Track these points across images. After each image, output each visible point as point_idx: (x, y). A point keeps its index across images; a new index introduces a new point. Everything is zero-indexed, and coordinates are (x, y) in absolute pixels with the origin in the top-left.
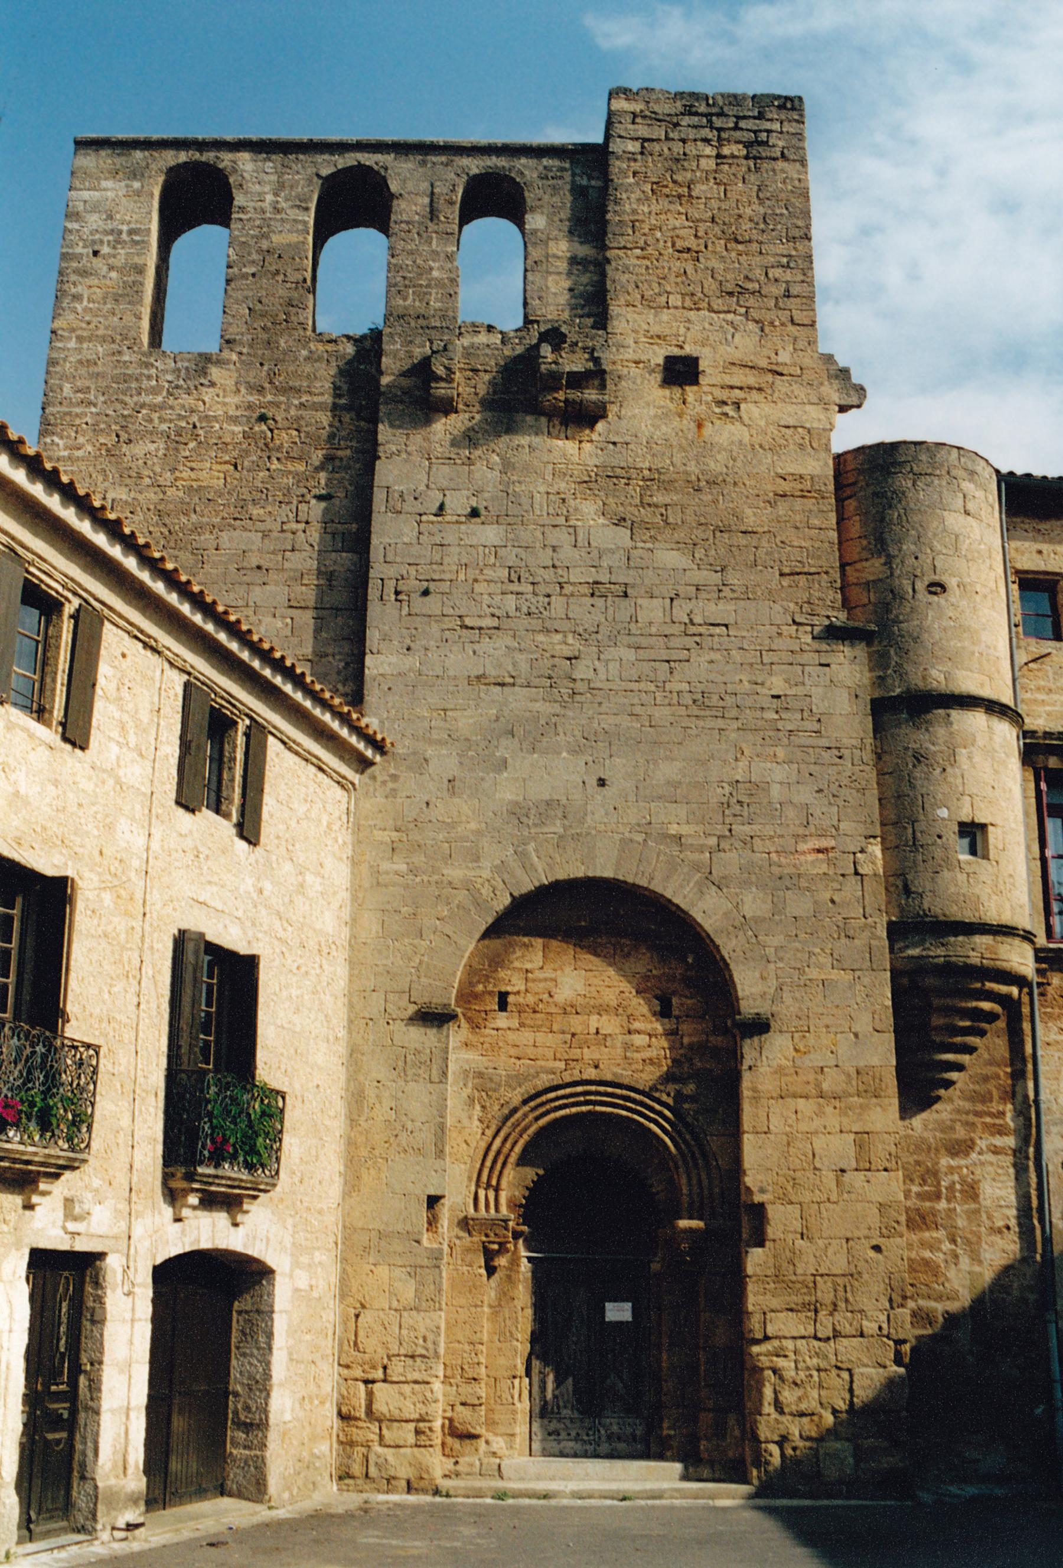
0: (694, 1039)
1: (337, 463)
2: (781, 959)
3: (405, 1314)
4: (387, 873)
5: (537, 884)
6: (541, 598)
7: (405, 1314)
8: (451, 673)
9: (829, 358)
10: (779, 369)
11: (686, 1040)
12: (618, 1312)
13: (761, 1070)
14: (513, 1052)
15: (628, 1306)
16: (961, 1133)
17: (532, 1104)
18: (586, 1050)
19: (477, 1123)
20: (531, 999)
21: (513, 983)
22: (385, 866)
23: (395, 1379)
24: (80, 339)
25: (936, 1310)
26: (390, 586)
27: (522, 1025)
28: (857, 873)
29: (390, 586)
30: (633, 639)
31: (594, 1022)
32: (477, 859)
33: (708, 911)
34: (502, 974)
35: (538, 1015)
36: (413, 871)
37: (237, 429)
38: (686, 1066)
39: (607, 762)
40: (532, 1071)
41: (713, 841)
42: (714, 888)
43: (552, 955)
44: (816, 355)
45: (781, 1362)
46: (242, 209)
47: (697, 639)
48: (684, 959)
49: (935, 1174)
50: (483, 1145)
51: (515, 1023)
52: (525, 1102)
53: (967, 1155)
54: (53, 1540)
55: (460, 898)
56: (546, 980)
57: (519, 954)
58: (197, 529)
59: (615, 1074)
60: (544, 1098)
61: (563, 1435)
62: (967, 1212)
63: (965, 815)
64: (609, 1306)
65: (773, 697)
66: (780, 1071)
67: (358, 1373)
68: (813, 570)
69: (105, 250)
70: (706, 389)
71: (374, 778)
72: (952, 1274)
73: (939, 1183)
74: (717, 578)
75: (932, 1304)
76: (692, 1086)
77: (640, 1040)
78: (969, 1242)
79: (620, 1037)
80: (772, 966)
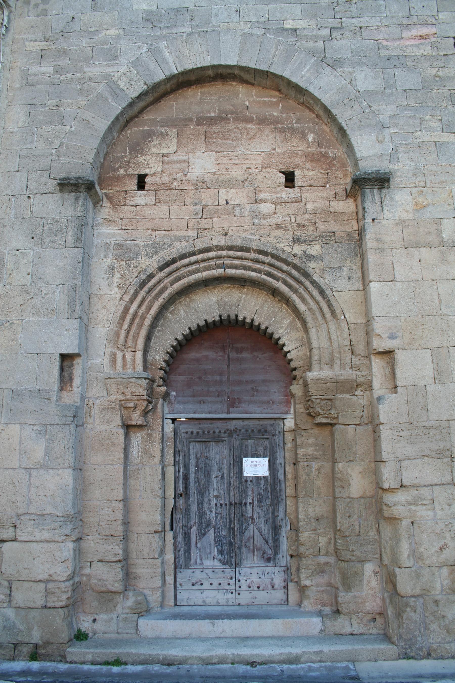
0: (318, 205)
2: (395, 125)
3: (34, 473)
4: (35, 75)
5: (168, 74)
7: (34, 473)
11: (309, 206)
12: (256, 467)
13: (384, 222)
14: (149, 225)
15: (265, 461)
17: (167, 270)
18: (216, 220)
19: (116, 289)
20: (166, 178)
21: (150, 165)
22: (33, 70)
23: (23, 539)
27: (158, 201)
31: (223, 195)
32: (115, 57)
34: (141, 159)
35: (174, 191)
36: (58, 71)
38: (311, 228)
40: (166, 241)
41: (326, 32)
42: (329, 69)
43: (185, 141)
45: (423, 513)
48: (304, 137)
50: (121, 308)
51: (151, 199)
52: (161, 269)
54: (257, 656)
55: (99, 90)
56: (179, 162)
57: (156, 141)
59: (243, 239)
60: (179, 264)
61: (206, 585)
66: (401, 223)
76: (317, 247)
77: (266, 208)
79: (248, 207)
80: (387, 131)
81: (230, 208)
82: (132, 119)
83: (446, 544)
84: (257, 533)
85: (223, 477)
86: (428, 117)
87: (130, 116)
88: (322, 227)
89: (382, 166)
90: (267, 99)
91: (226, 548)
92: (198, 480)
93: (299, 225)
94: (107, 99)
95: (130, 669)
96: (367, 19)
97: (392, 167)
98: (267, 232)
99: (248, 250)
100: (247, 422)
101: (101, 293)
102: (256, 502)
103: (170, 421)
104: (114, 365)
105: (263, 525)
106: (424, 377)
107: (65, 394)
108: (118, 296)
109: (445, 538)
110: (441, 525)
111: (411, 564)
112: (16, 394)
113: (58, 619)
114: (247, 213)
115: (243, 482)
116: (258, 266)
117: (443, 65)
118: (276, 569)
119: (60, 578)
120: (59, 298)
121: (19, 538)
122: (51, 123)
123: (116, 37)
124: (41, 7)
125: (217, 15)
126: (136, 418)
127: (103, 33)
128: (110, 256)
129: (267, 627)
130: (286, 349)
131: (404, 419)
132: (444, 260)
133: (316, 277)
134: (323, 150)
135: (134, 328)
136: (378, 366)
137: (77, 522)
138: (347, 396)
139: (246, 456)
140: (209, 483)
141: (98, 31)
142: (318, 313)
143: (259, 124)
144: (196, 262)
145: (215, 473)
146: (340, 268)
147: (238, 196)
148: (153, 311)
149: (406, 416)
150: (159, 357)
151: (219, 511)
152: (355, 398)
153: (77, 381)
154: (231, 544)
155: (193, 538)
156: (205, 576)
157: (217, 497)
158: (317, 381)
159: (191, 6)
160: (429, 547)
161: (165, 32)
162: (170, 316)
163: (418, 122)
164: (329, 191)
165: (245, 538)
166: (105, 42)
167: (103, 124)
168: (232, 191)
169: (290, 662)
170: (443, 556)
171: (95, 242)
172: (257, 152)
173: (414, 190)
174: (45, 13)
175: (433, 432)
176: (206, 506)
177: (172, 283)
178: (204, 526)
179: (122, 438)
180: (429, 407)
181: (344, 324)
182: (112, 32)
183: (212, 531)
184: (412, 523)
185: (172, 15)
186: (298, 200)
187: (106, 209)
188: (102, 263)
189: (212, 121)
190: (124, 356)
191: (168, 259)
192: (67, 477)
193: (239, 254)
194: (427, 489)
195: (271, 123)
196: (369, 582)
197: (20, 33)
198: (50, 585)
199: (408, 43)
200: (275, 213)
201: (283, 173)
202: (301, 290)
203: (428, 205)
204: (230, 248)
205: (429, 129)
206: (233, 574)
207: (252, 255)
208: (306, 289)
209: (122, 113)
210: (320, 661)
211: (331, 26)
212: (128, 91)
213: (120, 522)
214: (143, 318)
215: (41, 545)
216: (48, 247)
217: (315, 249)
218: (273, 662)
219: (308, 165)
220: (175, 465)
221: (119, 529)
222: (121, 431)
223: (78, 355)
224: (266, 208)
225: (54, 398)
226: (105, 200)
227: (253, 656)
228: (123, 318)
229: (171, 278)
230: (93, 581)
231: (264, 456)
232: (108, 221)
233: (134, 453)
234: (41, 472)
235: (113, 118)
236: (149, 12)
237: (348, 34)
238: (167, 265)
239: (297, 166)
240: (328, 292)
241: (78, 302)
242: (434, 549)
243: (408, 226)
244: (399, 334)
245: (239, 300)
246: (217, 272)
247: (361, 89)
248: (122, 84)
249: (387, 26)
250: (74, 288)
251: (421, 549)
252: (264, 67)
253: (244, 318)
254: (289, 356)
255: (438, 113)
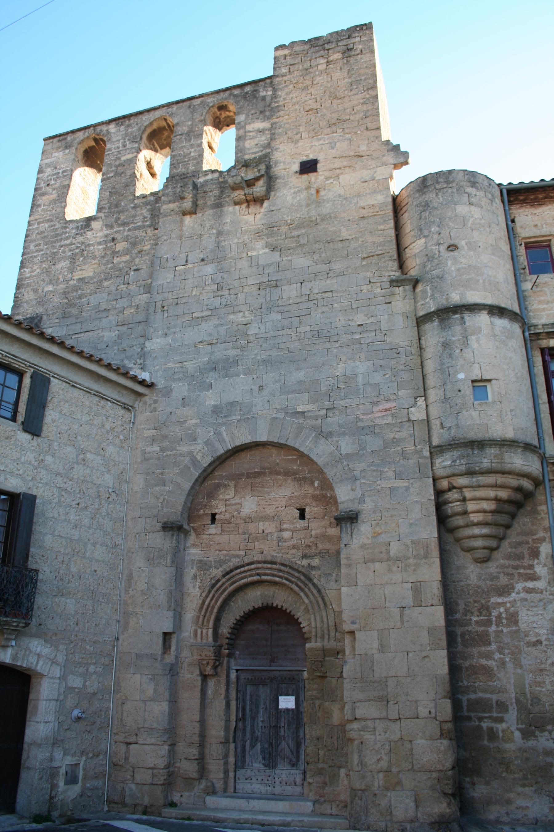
0: (318, 531)
1: (143, 253)
2: (364, 477)
3: (148, 703)
4: (149, 453)
5: (225, 449)
6: (232, 296)
7: (148, 703)
8: (186, 343)
9: (388, 142)
10: (360, 154)
11: (313, 533)
12: (287, 702)
13: (352, 546)
15: (292, 699)
16: (503, 580)
17: (227, 577)
18: (256, 543)
19: (198, 589)
20: (228, 516)
21: (219, 508)
22: (148, 449)
24: (39, 223)
25: (492, 700)
26: (159, 304)
27: (223, 531)
28: (409, 420)
29: (159, 304)
30: (280, 308)
31: (261, 526)
32: (195, 439)
33: (320, 452)
34: (214, 503)
36: (163, 450)
37: (101, 247)
38: (314, 548)
39: (265, 376)
40: (227, 558)
42: (323, 440)
44: (380, 143)
45: (368, 736)
46: (110, 150)
47: (315, 302)
48: (312, 484)
49: (488, 608)
50: (201, 602)
51: (219, 530)
52: (224, 576)
53: (509, 594)
54: (266, 820)
55: (186, 462)
56: (236, 504)
57: (222, 491)
58: (80, 298)
59: (272, 556)
60: (233, 573)
61: (254, 780)
62: (509, 632)
63: (476, 374)
64: (281, 698)
65: (359, 325)
66: (363, 547)
67: (121, 738)
68: (380, 252)
69: (52, 182)
70: (321, 173)
71: (145, 403)
72: (501, 675)
73: (490, 614)
74: (325, 268)
75: (488, 696)
78: (512, 653)
81: (265, 536)
82: (208, 475)
83: (381, 757)
84: (286, 747)
85: (266, 709)
86: (386, 469)
87: (207, 474)
88: (320, 546)
89: (354, 507)
90: (290, 457)
91: (267, 756)
92: (251, 710)
93: (306, 546)
94: (190, 468)
95: (195, 822)
96: (350, 400)
97: (360, 507)
98: (287, 551)
99: (275, 563)
100: (281, 673)
101: (189, 591)
102: (286, 726)
103: (235, 671)
104: (195, 637)
105: (290, 742)
106: (372, 649)
107: (166, 656)
108: (199, 594)
109: (381, 753)
110: (378, 745)
111: (360, 769)
112: (139, 656)
113: (159, 791)
114: (275, 539)
115: (278, 712)
116: (281, 574)
117: (399, 430)
118: (297, 772)
119: (160, 767)
120: (162, 598)
121: (139, 742)
122: (158, 485)
123: (196, 425)
124: (153, 406)
125: (256, 405)
126: (209, 670)
127: (188, 422)
128: (195, 568)
129: (281, 806)
130: (302, 626)
131: (358, 675)
132: (390, 570)
133: (315, 581)
134: (324, 492)
135: (208, 614)
136: (347, 640)
137: (171, 734)
138: (332, 659)
139: (281, 695)
140: (258, 712)
141: (185, 421)
142: (315, 605)
143: (285, 476)
144: (245, 571)
145: (262, 706)
146: (331, 575)
147: (269, 527)
148: (219, 603)
149: (360, 674)
150: (225, 630)
151: (264, 731)
152: (337, 660)
153: (173, 648)
154: (270, 753)
155: (247, 748)
156: (253, 774)
157: (262, 722)
158: (311, 649)
159: (240, 400)
160: (370, 759)
161: (224, 420)
162: (232, 604)
163: (379, 473)
164: (326, 522)
165: (279, 750)
166: (189, 428)
167: (187, 486)
168: (267, 523)
169: (284, 825)
170: (379, 765)
171: (186, 559)
172: (282, 495)
173: (373, 523)
174: (155, 410)
175: (376, 684)
176: (256, 727)
177: (231, 585)
178: (255, 740)
179: (199, 683)
180: (375, 668)
181: (331, 612)
182: (194, 421)
183: (259, 744)
184: (362, 743)
185: (229, 408)
186: (306, 529)
187: (192, 537)
188: (190, 572)
189: (257, 475)
190: (202, 632)
191: (228, 569)
192: (165, 706)
193: (269, 566)
194: (371, 721)
195: (292, 475)
196: (343, 781)
197: (141, 425)
198: (155, 771)
199: (376, 415)
200: (292, 538)
201: (298, 509)
202: (306, 590)
203: (381, 533)
204: (265, 562)
205: (387, 478)
206: (270, 774)
207: (278, 567)
208: (309, 589)
209: (199, 477)
210: (302, 827)
211: (327, 407)
212: (202, 463)
213: (197, 735)
214: (213, 608)
215: (150, 746)
216: (157, 566)
217: (316, 562)
218: (275, 825)
219: (314, 504)
220: (237, 700)
221: (196, 739)
222: (199, 678)
223: (174, 633)
224: (286, 535)
225: (159, 659)
226: (192, 531)
227: (263, 820)
228: (201, 608)
229: (230, 582)
230: (181, 771)
231: (292, 695)
232: (194, 545)
233: (210, 692)
234: (151, 703)
235: (193, 481)
236: (215, 406)
237: (337, 413)
238: (228, 573)
239: (307, 505)
240: (323, 591)
241: (173, 600)
242: (373, 761)
243: (368, 548)
244: (358, 621)
245: (274, 594)
246: (255, 578)
247: (343, 453)
248: (199, 458)
249: (364, 404)
250: (171, 592)
251: (366, 760)
252: (283, 441)
253: (277, 605)
254: (304, 630)
255: (393, 466)
